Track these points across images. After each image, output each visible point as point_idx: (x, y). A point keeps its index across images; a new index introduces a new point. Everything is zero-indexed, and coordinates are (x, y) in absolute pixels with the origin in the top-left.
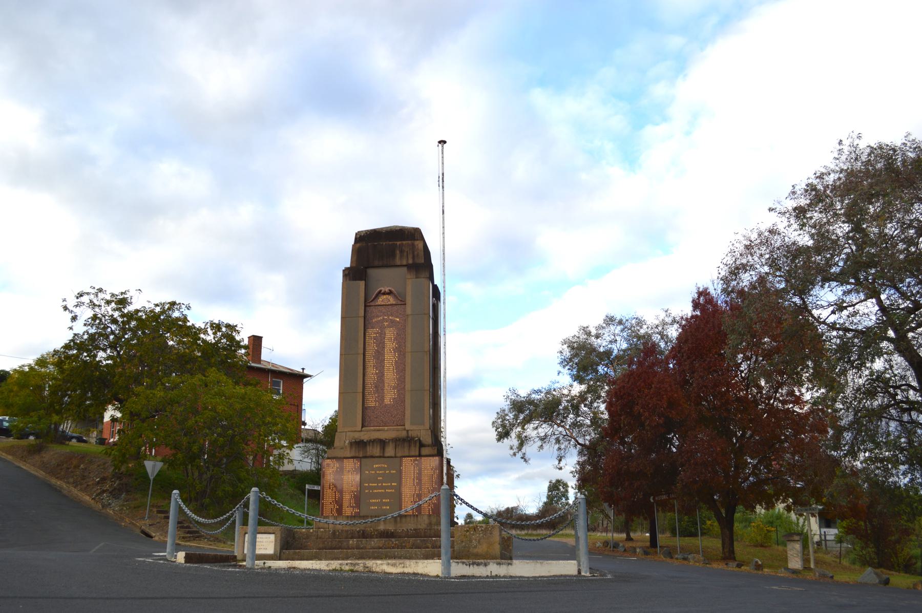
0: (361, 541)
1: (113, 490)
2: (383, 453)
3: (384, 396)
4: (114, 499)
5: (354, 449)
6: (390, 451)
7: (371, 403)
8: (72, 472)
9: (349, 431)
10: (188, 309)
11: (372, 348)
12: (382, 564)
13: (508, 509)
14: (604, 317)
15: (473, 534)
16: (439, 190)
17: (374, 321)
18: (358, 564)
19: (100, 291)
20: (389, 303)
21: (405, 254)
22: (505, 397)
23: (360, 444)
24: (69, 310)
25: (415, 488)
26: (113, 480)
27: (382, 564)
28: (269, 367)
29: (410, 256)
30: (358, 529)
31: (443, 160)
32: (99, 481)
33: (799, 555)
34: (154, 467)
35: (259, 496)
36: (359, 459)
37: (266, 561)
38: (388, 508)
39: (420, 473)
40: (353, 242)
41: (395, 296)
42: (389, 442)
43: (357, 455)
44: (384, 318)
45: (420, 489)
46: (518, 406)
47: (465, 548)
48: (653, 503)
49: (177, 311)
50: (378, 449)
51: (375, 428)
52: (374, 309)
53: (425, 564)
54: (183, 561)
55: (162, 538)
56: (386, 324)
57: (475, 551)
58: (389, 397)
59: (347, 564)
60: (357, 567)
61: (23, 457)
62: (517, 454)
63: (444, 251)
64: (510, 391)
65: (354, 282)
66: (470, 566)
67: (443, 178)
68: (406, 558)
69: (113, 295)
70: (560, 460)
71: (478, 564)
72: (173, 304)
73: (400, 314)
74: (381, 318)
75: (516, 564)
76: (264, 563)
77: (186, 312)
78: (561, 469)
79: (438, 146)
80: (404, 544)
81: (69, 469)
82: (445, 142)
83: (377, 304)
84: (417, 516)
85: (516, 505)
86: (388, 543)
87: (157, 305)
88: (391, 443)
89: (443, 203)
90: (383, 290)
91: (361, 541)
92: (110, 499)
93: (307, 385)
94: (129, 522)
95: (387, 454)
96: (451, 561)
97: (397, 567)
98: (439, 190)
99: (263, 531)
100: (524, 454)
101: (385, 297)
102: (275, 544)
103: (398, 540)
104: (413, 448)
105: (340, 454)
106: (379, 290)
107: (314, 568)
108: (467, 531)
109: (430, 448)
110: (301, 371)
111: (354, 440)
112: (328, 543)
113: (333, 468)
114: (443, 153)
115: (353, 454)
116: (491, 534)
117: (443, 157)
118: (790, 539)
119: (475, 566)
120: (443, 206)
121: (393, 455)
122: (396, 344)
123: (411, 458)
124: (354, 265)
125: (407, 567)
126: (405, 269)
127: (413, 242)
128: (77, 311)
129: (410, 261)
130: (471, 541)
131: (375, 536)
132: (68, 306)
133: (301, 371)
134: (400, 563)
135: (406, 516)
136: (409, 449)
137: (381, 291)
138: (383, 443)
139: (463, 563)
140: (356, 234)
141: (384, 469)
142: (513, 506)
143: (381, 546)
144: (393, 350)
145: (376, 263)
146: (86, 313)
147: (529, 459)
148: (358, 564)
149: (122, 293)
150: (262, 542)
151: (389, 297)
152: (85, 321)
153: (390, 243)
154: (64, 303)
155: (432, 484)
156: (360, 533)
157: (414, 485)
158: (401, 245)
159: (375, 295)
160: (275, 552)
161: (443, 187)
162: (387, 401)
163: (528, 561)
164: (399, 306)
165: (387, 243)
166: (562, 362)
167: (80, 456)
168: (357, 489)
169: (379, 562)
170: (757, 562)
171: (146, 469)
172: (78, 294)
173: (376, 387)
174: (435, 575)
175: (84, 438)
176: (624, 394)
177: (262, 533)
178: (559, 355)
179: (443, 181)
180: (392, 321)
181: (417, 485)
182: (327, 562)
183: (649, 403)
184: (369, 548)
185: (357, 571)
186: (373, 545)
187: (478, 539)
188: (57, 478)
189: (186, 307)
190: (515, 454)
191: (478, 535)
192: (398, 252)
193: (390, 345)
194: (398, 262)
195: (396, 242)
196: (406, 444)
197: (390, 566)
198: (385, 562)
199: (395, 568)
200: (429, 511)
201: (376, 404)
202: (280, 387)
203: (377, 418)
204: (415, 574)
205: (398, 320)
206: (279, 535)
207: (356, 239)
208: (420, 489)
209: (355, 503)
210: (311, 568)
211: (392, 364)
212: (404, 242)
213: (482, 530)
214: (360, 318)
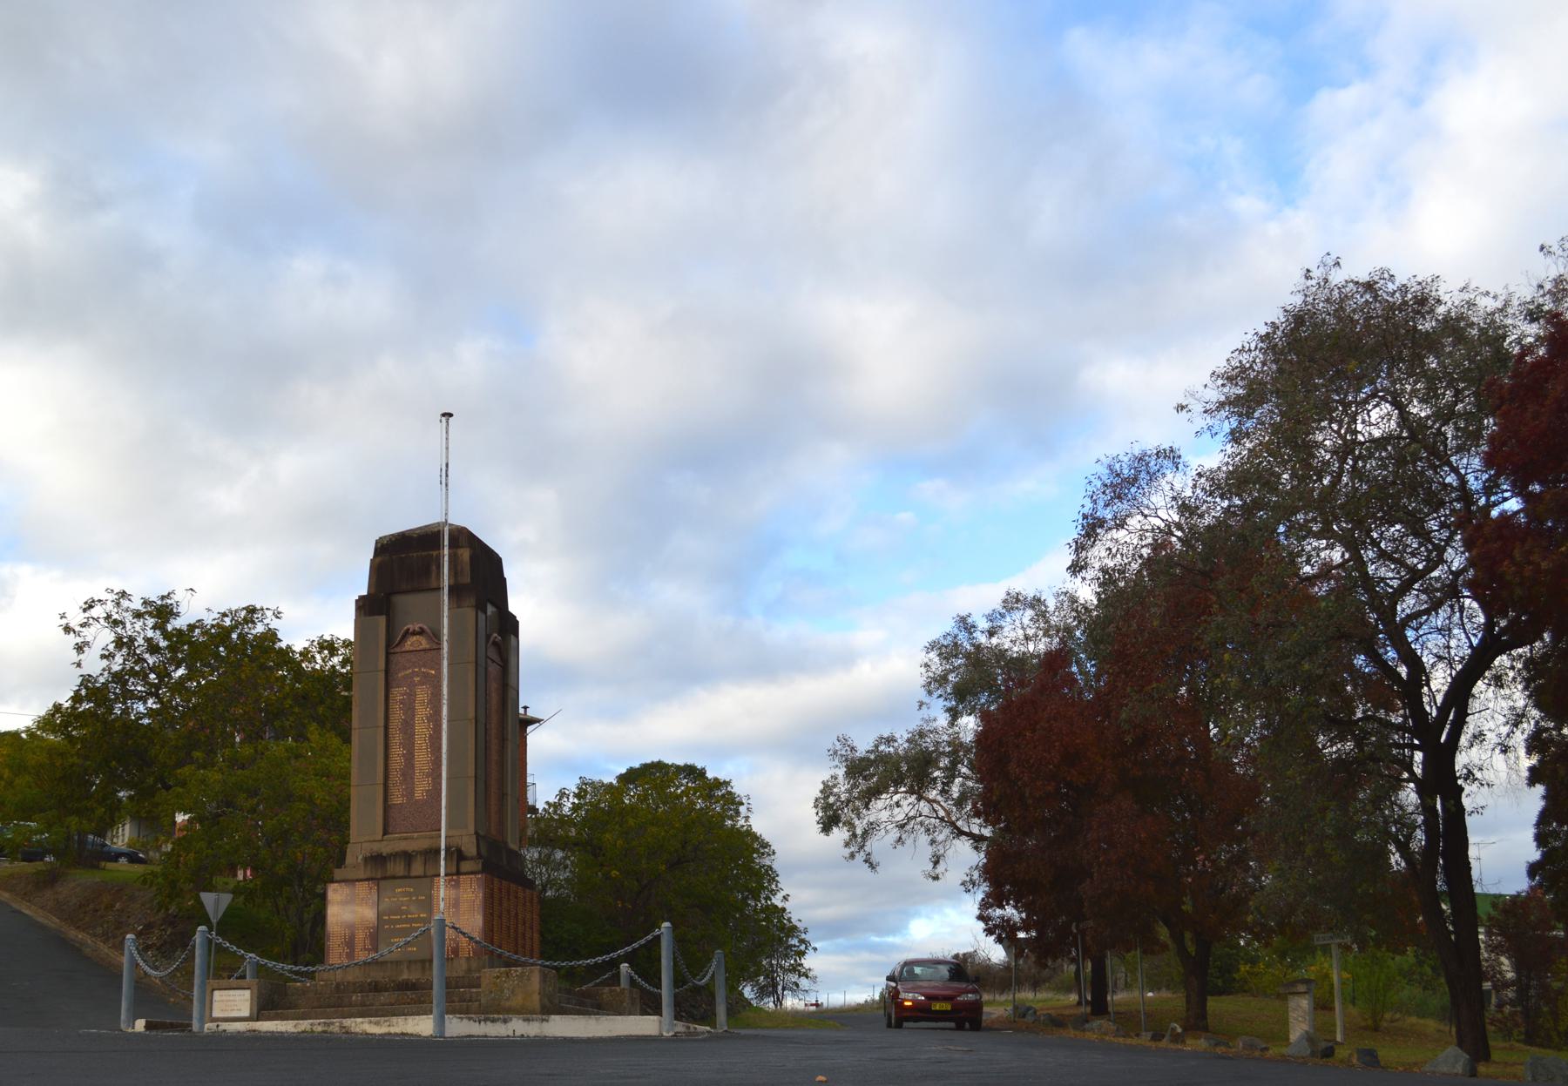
0: (367, 996)
1: (162, 945)
2: (409, 871)
4: (163, 959)
5: (369, 867)
7: (397, 798)
8: (102, 917)
9: (365, 842)
10: (278, 617)
11: (397, 715)
12: (362, 1023)
14: (1003, 596)
15: (505, 981)
16: (441, 489)
17: (400, 675)
19: (123, 596)
20: (421, 647)
22: (831, 752)
23: (377, 860)
24: (75, 632)
26: (163, 927)
27: (362, 1023)
30: (369, 980)
31: (447, 443)
32: (142, 930)
33: (1307, 1018)
34: (217, 902)
35: (208, 937)
36: (376, 881)
40: (371, 555)
42: (417, 854)
43: (374, 876)
46: (856, 768)
50: (402, 866)
52: (400, 658)
54: (143, 1030)
56: (417, 679)
57: (508, 1004)
59: (319, 1024)
60: (332, 1027)
61: (25, 894)
62: (857, 855)
64: (839, 741)
66: (480, 1023)
67: (447, 471)
68: (394, 1015)
69: (146, 602)
70: (936, 863)
71: (493, 1021)
72: (252, 610)
75: (554, 1020)
76: (218, 1026)
77: (274, 624)
78: (936, 878)
79: (441, 421)
80: (422, 999)
81: (97, 911)
82: (451, 415)
83: (403, 649)
84: (452, 959)
87: (225, 615)
89: (447, 510)
90: (411, 627)
92: (157, 960)
94: (183, 997)
95: (413, 874)
96: (446, 1016)
98: (441, 489)
99: (235, 986)
100: (869, 854)
101: (415, 638)
102: (251, 1003)
105: (351, 876)
106: (405, 628)
107: (279, 1030)
108: (498, 977)
109: (472, 862)
114: (447, 432)
115: (368, 874)
117: (447, 439)
118: (1292, 991)
119: (488, 1023)
121: (423, 874)
122: (431, 709)
128: (89, 633)
130: (502, 991)
132: (71, 625)
134: (386, 1021)
137: (409, 629)
138: (408, 857)
139: (470, 1019)
140: (377, 542)
141: (410, 894)
142: (965, 951)
143: (393, 1001)
144: (427, 718)
146: (103, 637)
147: (878, 864)
148: (333, 1023)
149: (163, 598)
150: (234, 1001)
152: (103, 649)
153: (423, 553)
154: (64, 622)
160: (251, 1013)
161: (447, 485)
162: (418, 796)
165: (419, 554)
166: (930, 683)
167: (116, 888)
169: (359, 1020)
170: (1174, 1029)
171: (205, 910)
172: (86, 603)
173: (403, 775)
175: (141, 855)
177: (234, 989)
178: (923, 670)
179: (447, 476)
187: (511, 988)
188: (78, 927)
190: (852, 856)
191: (511, 983)
193: (422, 712)
195: (431, 553)
197: (372, 1025)
198: (367, 1019)
200: (469, 951)
203: (404, 820)
204: (403, 1034)
205: (433, 672)
206: (255, 991)
213: (517, 975)
214: (379, 673)
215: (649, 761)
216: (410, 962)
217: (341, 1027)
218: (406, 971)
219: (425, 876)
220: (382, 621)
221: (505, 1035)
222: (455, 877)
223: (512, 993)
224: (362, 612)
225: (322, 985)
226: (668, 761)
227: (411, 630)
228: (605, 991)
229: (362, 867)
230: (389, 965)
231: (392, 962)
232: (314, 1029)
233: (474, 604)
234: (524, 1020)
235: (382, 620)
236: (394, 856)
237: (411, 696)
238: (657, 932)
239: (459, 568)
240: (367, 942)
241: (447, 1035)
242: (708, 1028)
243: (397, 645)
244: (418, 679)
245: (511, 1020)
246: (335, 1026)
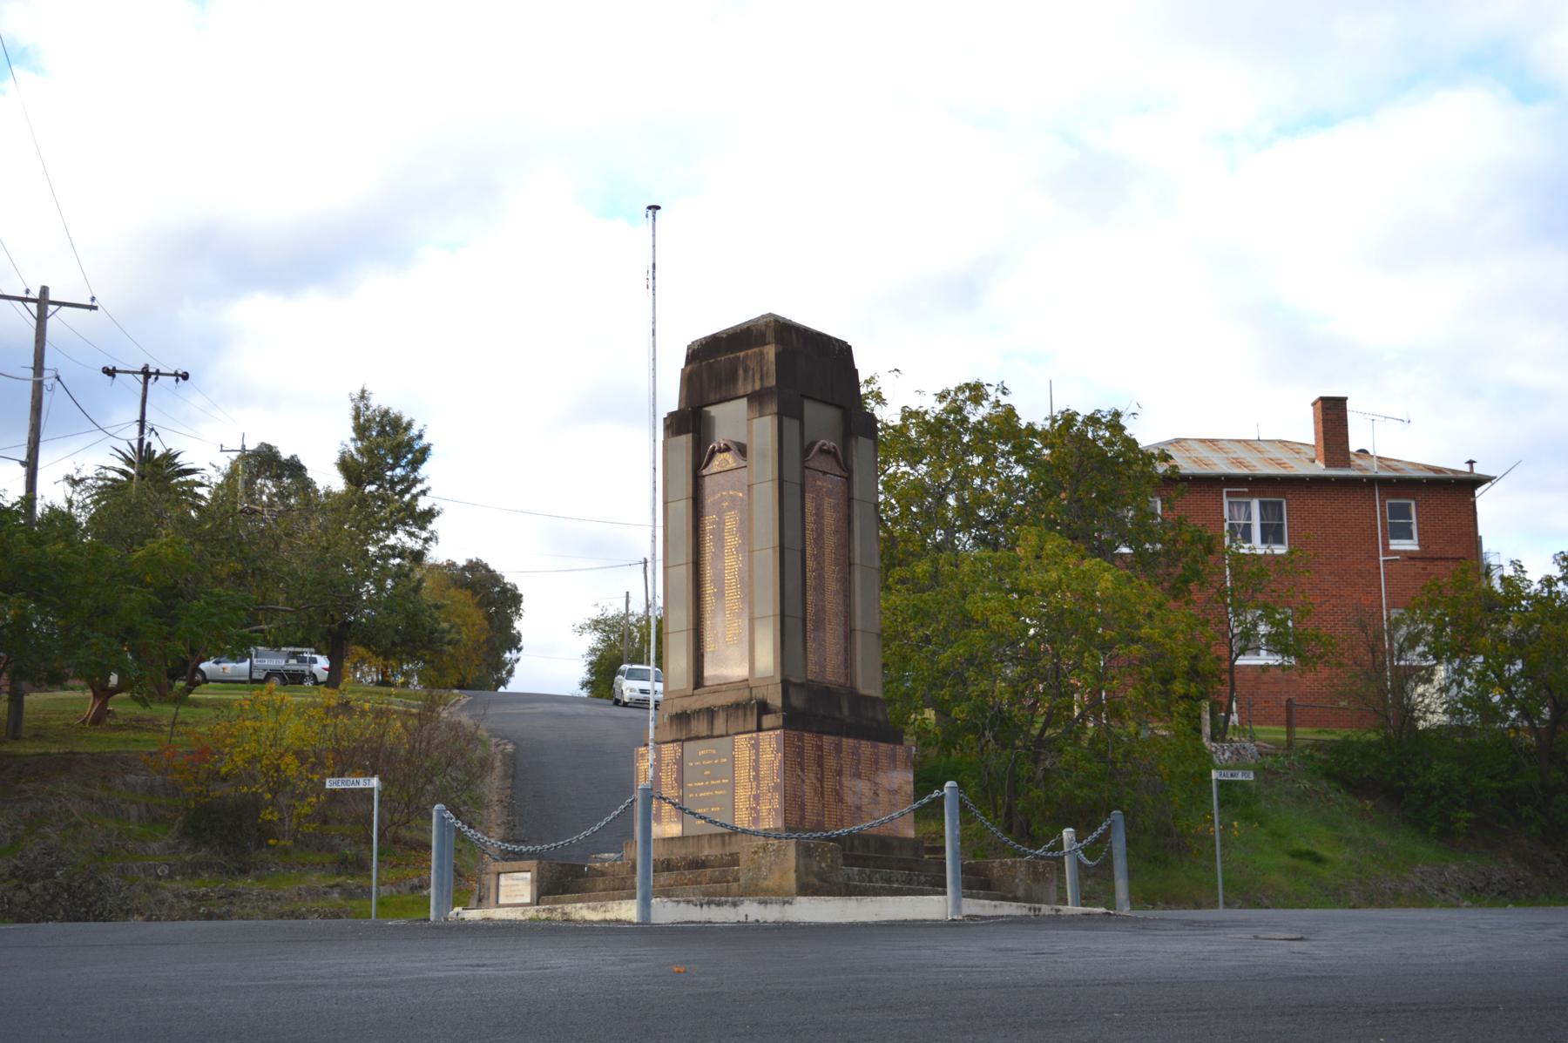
2: (712, 729)
12: (581, 908)
20: (727, 467)
27: (581, 908)
28: (1375, 470)
36: (681, 743)
39: (757, 761)
43: (678, 737)
44: (722, 495)
45: (758, 787)
53: (629, 905)
59: (544, 910)
63: (654, 394)
66: (702, 906)
71: (719, 904)
75: (800, 903)
77: (1004, 400)
79: (647, 216)
80: (699, 879)
82: (658, 208)
83: (712, 471)
88: (721, 712)
89: (654, 318)
93: (1485, 500)
95: (716, 733)
99: (517, 869)
104: (749, 718)
108: (756, 852)
116: (785, 855)
119: (713, 907)
121: (724, 733)
124: (683, 407)
130: (759, 869)
133: (1466, 468)
136: (745, 721)
137: (714, 447)
139: (688, 902)
143: (672, 882)
145: (713, 397)
148: (555, 910)
151: (726, 455)
157: (750, 779)
159: (706, 457)
161: (654, 290)
165: (726, 357)
179: (654, 278)
181: (754, 779)
185: (554, 920)
187: (769, 864)
196: (740, 712)
198: (585, 905)
202: (1411, 518)
204: (618, 921)
208: (758, 787)
211: (734, 575)
212: (750, 352)
218: (707, 846)
219: (727, 735)
220: (685, 440)
221: (735, 921)
222: (754, 735)
223: (770, 870)
224: (670, 431)
225: (619, 865)
227: (716, 448)
228: (994, 864)
229: (668, 728)
230: (691, 841)
231: (693, 837)
232: (540, 916)
233: (776, 410)
234: (760, 903)
236: (698, 712)
237: (720, 523)
238: (936, 793)
241: (653, 921)
242: (1103, 910)
244: (727, 504)
245: (742, 902)
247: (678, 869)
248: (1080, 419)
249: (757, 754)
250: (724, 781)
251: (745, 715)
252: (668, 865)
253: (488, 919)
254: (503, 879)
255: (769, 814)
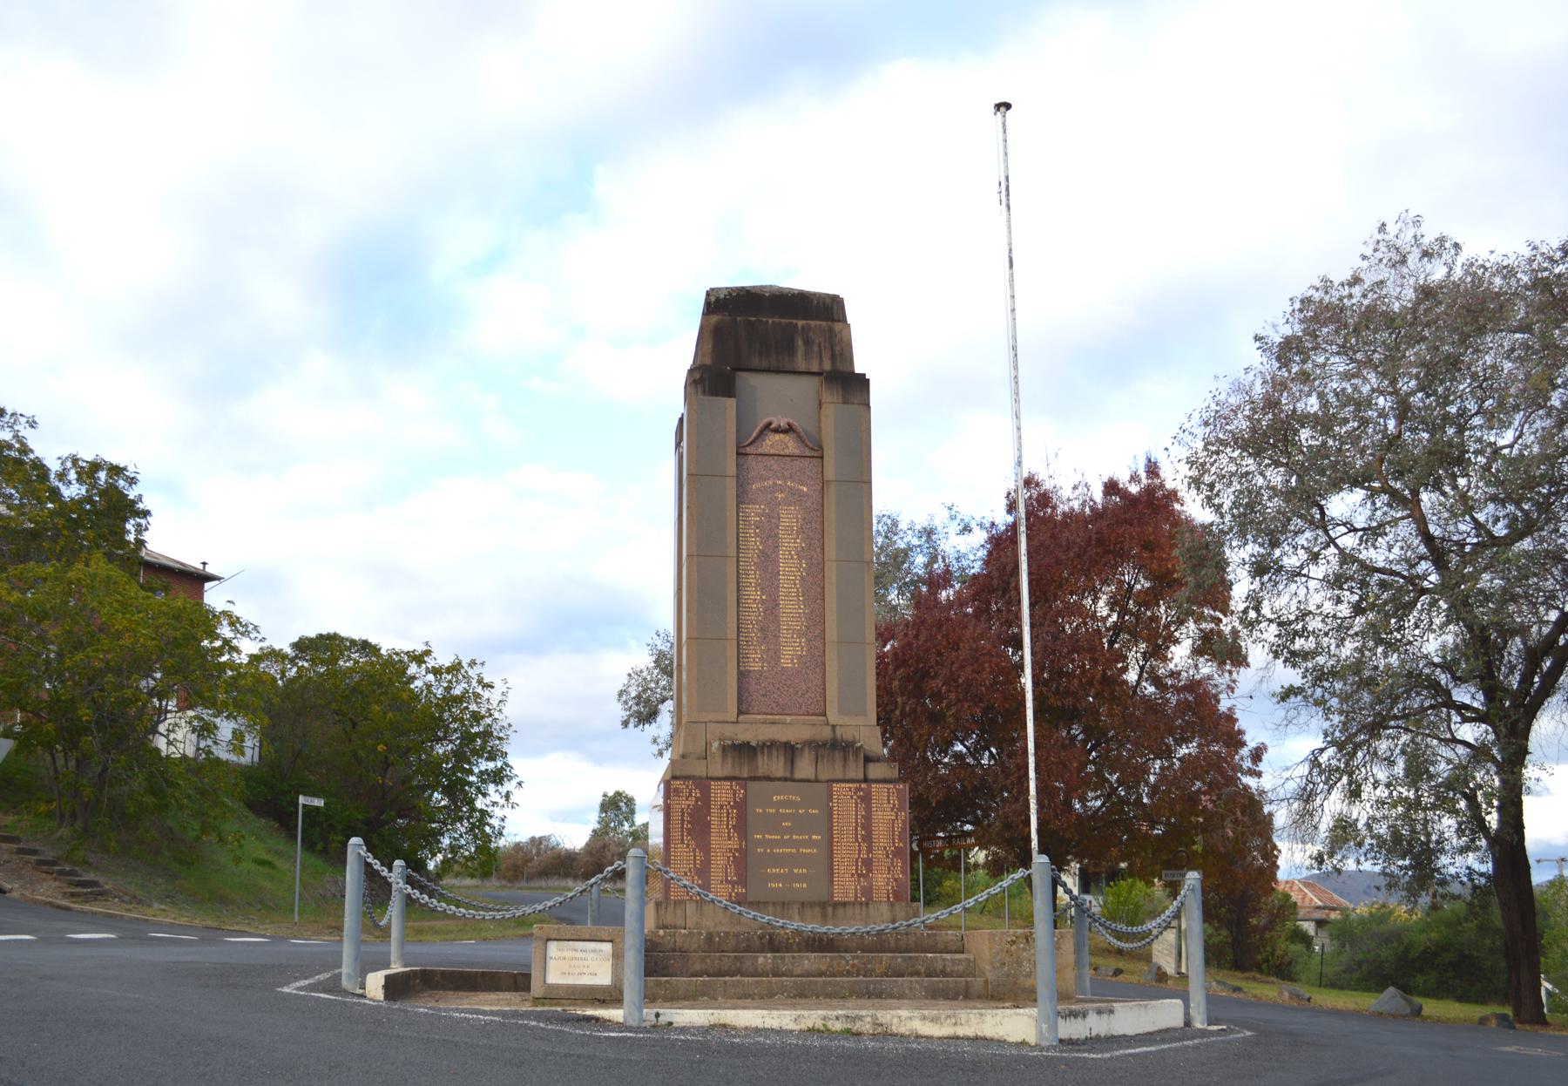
0: (782, 958)
3: (779, 650)
6: (805, 768)
10: (33, 427)
11: (754, 543)
12: (911, 1018)
13: (533, 839)
15: (1024, 949)
18: (860, 1018)
20: (787, 452)
21: (816, 349)
25: (859, 846)
27: (911, 1018)
29: (826, 356)
37: (661, 1011)
38: (805, 885)
39: (868, 818)
41: (799, 437)
42: (802, 749)
43: (737, 773)
44: (775, 484)
45: (870, 850)
47: (1008, 976)
48: (918, 852)
49: (9, 429)
50: (781, 763)
51: (764, 717)
53: (998, 1019)
54: (380, 995)
55: (27, 893)
58: (791, 652)
59: (837, 1018)
65: (714, 398)
73: (809, 477)
74: (771, 482)
76: (657, 1015)
77: (25, 432)
80: (870, 966)
82: (1008, 106)
83: (760, 451)
85: (547, 834)
86: (838, 964)
89: (1010, 244)
91: (782, 958)
95: (799, 775)
97: (941, 1023)
99: (587, 937)
101: (777, 437)
103: (858, 957)
107: (767, 1026)
108: (1013, 942)
110: (201, 567)
111: (730, 742)
112: (713, 961)
113: (687, 799)
115: (728, 771)
120: (1010, 250)
121: (812, 777)
123: (851, 785)
124: (708, 361)
125: (961, 1024)
126: (815, 381)
127: (830, 323)
129: (827, 366)
130: (1019, 964)
131: (795, 947)
133: (201, 567)
134: (949, 1017)
135: (844, 904)
136: (844, 766)
137: (770, 424)
138: (790, 751)
140: (708, 294)
143: (824, 968)
155: (894, 839)
156: (764, 941)
157: (857, 840)
158: (806, 329)
161: (1008, 207)
162: (786, 662)
163: (1130, 1004)
164: (808, 459)
168: (741, 845)
169: (904, 1013)
174: (1020, 1040)
176: (911, 657)
180: (793, 492)
182: (795, 1013)
183: (959, 677)
184: (799, 972)
186: (806, 967)
189: (28, 422)
190: (661, 754)
192: (800, 343)
193: (789, 544)
194: (802, 366)
195: (794, 321)
196: (838, 755)
198: (916, 1013)
199: (939, 1026)
201: (763, 667)
204: (976, 1039)
205: (805, 489)
207: (708, 304)
208: (870, 850)
209: (736, 874)
210: (761, 1026)
211: (795, 584)
212: (813, 323)
215: (324, 632)
216: (803, 904)
217: (875, 1024)
219: (817, 781)
226: (344, 634)
231: (774, 904)
235: (730, 403)
236: (770, 746)
237: (772, 519)
239: (837, 348)
240: (731, 870)
243: (751, 443)
246: (869, 1017)
247: (788, 949)
248: (32, 456)
249: (868, 809)
250: (814, 837)
251: (845, 759)
252: (771, 940)
253: (724, 1026)
254: (553, 948)
255: (888, 884)
